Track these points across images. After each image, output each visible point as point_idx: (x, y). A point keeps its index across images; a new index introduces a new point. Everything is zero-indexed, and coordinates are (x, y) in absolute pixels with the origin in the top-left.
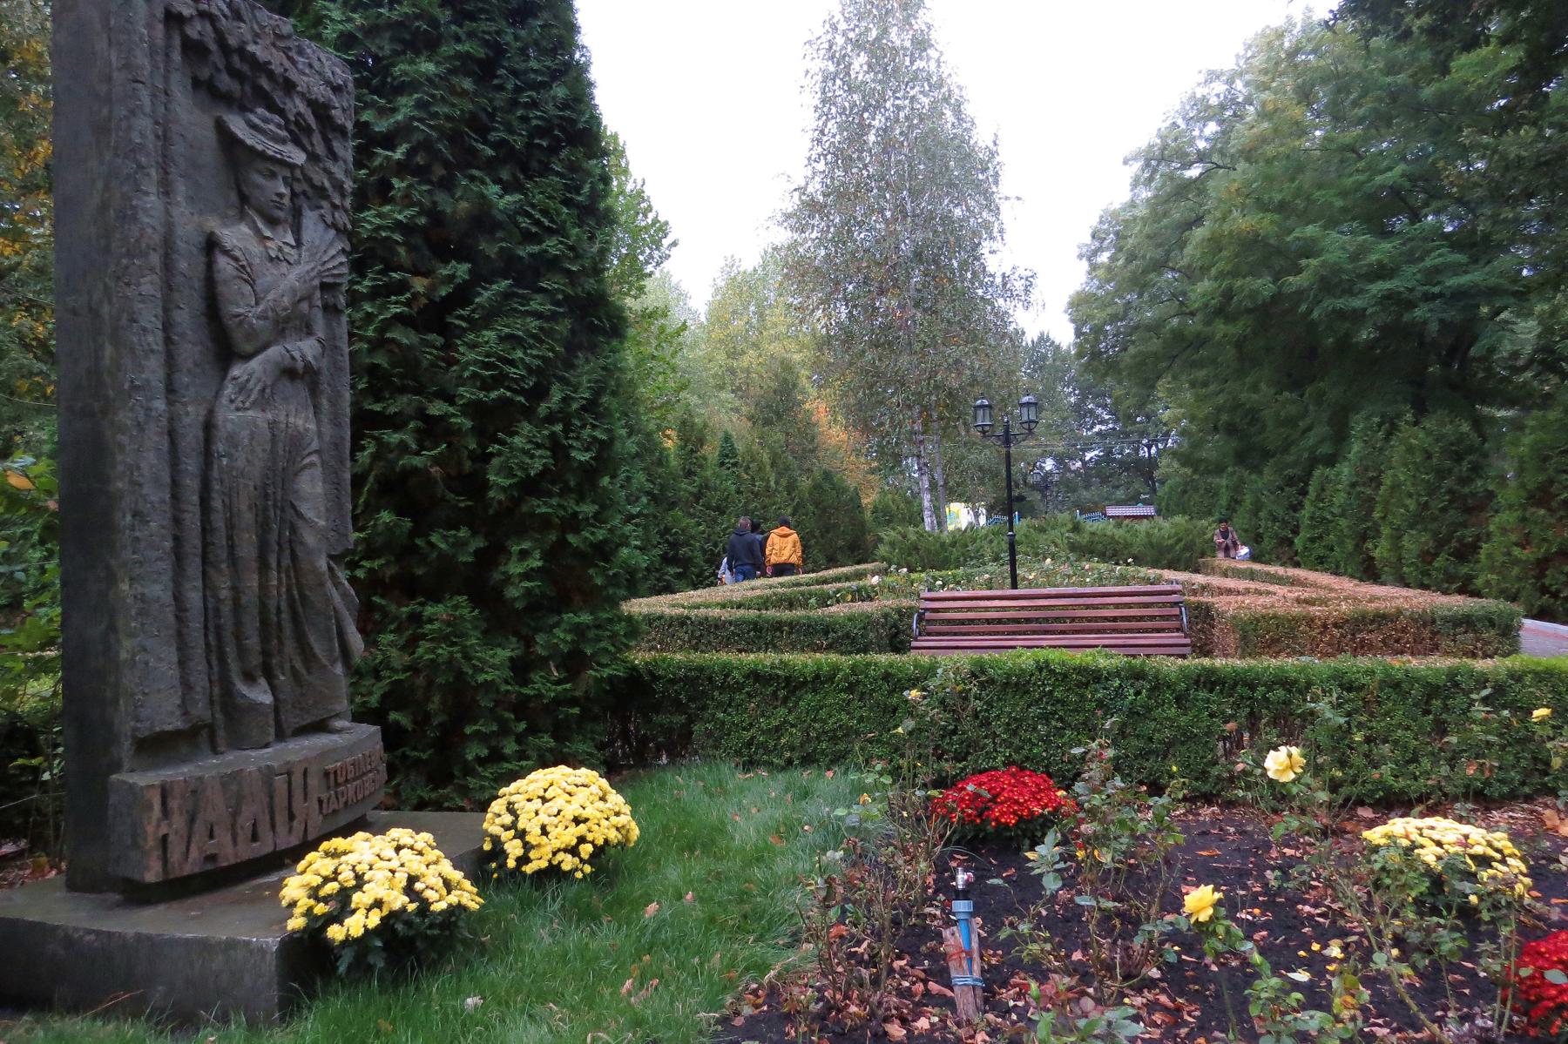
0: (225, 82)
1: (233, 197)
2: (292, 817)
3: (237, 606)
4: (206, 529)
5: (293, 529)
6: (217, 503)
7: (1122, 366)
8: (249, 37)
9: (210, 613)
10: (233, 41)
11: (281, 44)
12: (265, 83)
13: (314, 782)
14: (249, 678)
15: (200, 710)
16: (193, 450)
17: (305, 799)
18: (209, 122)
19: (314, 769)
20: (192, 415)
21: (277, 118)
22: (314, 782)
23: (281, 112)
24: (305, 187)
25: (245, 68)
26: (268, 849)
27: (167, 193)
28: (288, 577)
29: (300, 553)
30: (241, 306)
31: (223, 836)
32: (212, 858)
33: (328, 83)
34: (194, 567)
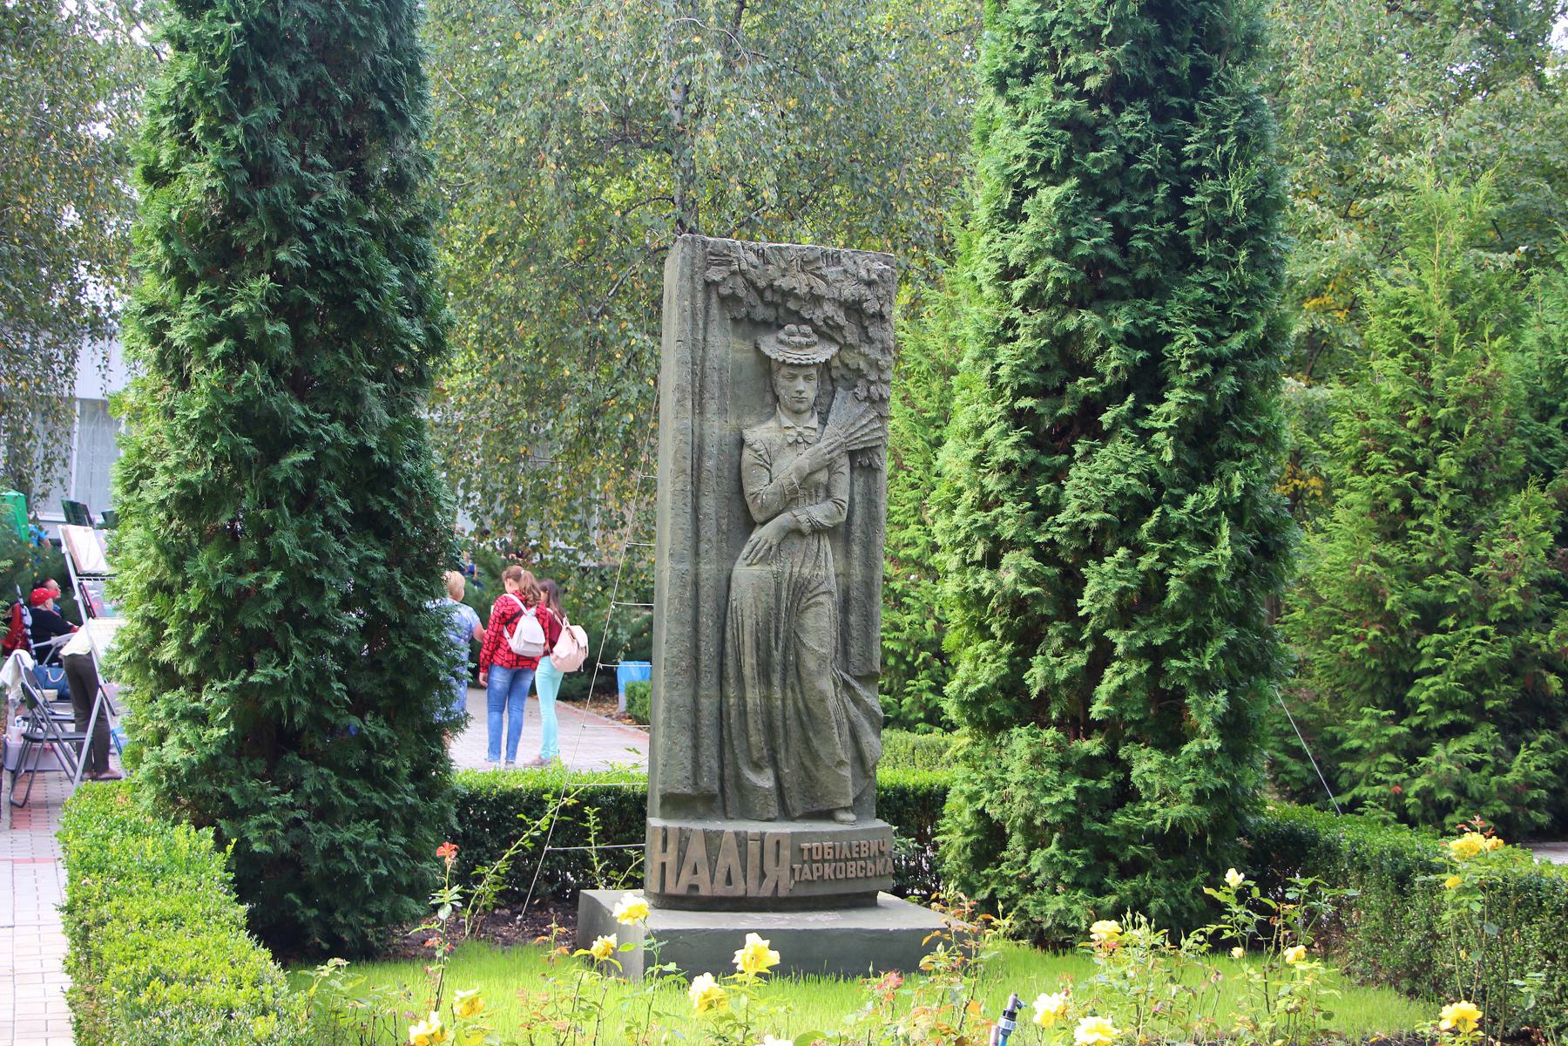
0: (761, 312)
1: (769, 398)
2: (763, 875)
3: (743, 713)
4: (722, 653)
5: (798, 656)
6: (729, 635)
7: (1193, 688)
8: (777, 274)
9: (721, 715)
10: (762, 283)
11: (809, 268)
12: (792, 305)
13: (786, 853)
14: (757, 767)
15: (709, 782)
16: (1545, 341)
17: (663, 865)
18: (748, 345)
19: (785, 843)
20: (708, 569)
21: (807, 329)
22: (786, 853)
23: (810, 322)
24: (844, 371)
25: (778, 299)
26: (740, 892)
27: (701, 413)
28: (793, 690)
29: (804, 675)
30: (761, 488)
31: (704, 874)
32: (694, 887)
33: (860, 281)
34: (708, 680)
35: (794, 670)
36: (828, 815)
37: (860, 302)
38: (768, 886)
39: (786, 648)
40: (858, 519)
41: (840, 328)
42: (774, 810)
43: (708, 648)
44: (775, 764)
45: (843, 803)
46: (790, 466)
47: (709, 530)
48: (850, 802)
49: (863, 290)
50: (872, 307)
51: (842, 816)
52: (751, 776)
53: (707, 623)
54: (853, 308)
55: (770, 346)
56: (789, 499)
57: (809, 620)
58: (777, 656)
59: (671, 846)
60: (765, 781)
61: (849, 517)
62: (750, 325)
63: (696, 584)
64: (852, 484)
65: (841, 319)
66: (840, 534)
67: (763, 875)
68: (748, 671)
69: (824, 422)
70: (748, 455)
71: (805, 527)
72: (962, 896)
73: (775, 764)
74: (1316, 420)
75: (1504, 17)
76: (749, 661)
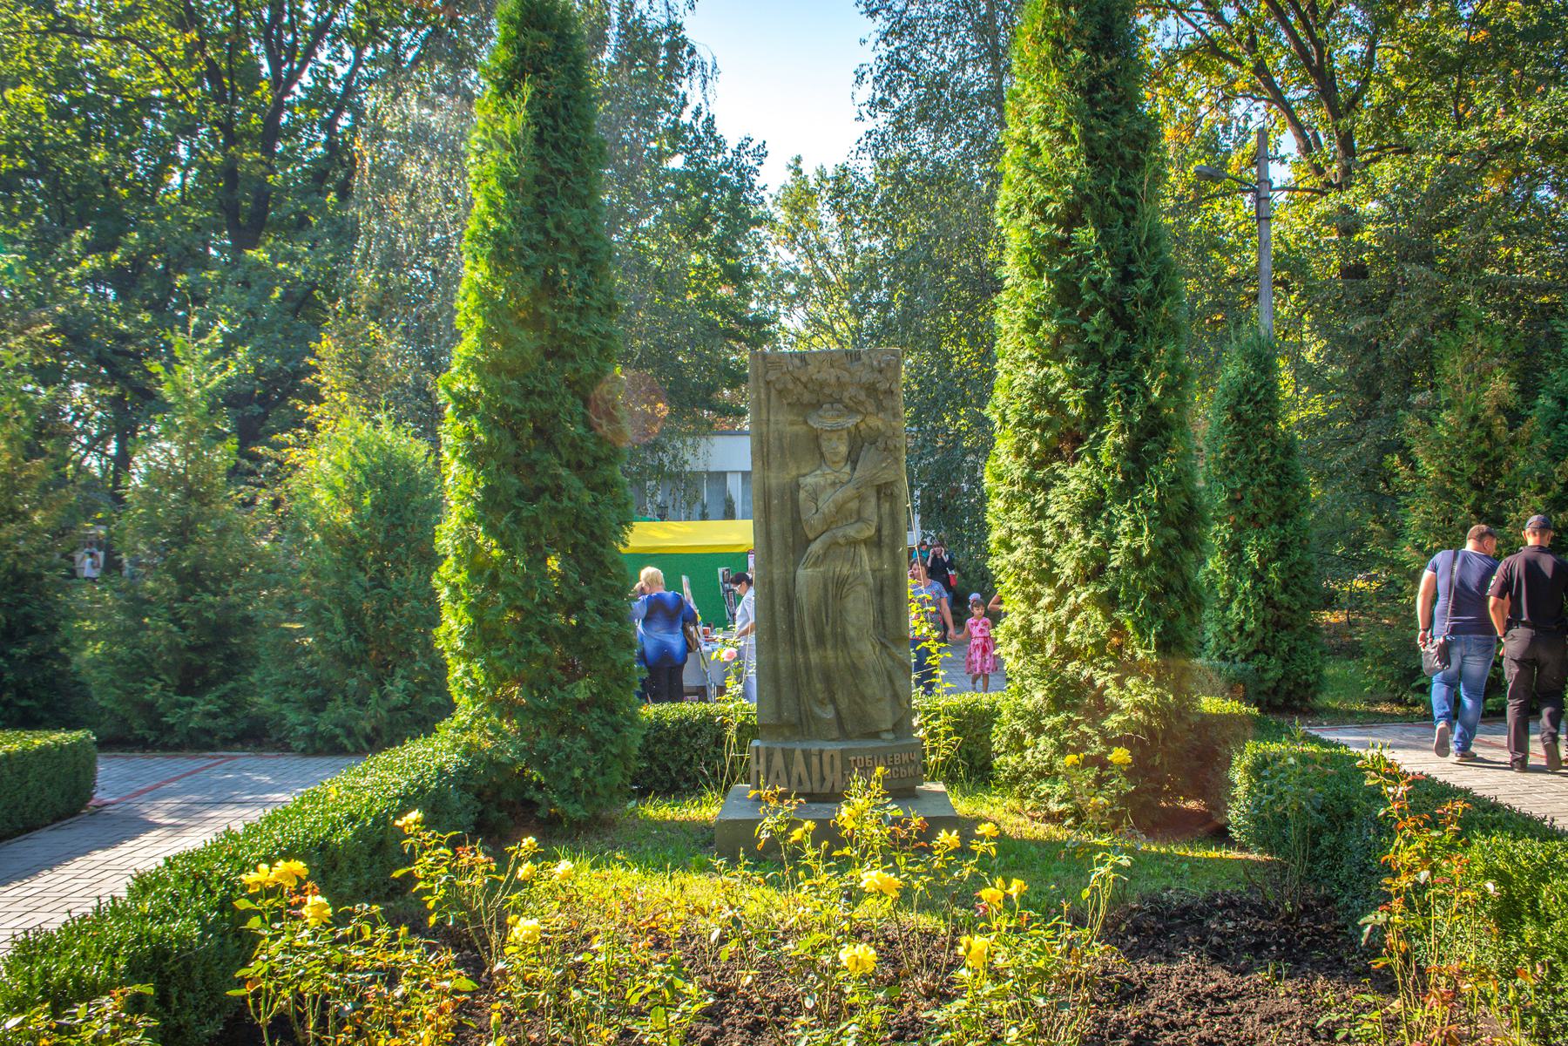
0: (807, 397)
2: (823, 779)
14: (821, 703)
20: (777, 572)
30: (812, 519)
35: (842, 641)
36: (876, 735)
37: (874, 384)
38: (828, 784)
39: (835, 623)
40: (886, 532)
41: (862, 403)
42: (835, 734)
43: (782, 626)
44: (833, 701)
45: (884, 727)
46: (827, 503)
47: (776, 547)
48: (890, 726)
49: (876, 375)
50: (883, 386)
51: (885, 736)
52: (817, 710)
53: (780, 609)
54: (871, 390)
55: (815, 423)
56: (829, 524)
57: (850, 603)
58: (828, 630)
59: (762, 760)
60: (828, 713)
61: (879, 530)
62: (805, 408)
63: (771, 583)
64: (879, 507)
65: (862, 396)
66: (876, 543)
67: (823, 779)
68: (809, 641)
69: (854, 469)
70: (802, 495)
71: (841, 541)
72: (1550, 494)
73: (833, 701)
74: (256, 609)
75: (1106, 11)
76: (809, 634)
